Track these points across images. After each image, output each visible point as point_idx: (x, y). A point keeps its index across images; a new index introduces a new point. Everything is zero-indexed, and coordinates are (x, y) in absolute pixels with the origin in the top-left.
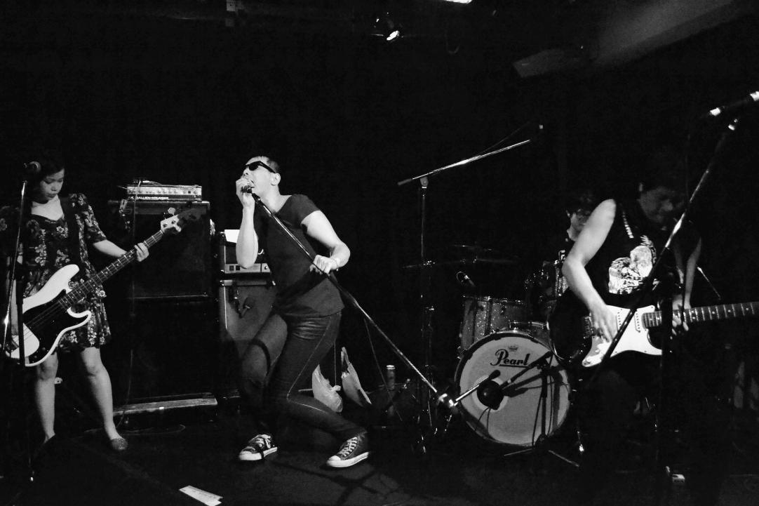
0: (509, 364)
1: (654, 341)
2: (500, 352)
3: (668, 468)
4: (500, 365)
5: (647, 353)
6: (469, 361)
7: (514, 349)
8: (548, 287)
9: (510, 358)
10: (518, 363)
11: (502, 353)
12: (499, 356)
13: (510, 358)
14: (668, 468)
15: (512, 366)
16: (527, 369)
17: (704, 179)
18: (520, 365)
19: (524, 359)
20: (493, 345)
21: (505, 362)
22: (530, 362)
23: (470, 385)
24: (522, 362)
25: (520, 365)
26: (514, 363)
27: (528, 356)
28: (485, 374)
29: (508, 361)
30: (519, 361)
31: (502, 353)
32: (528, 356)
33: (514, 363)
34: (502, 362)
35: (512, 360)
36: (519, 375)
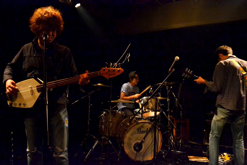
4: (139, 133)
10: (144, 132)
12: (138, 131)
21: (140, 132)
24: (145, 131)
25: (145, 132)
30: (145, 131)
34: (139, 132)
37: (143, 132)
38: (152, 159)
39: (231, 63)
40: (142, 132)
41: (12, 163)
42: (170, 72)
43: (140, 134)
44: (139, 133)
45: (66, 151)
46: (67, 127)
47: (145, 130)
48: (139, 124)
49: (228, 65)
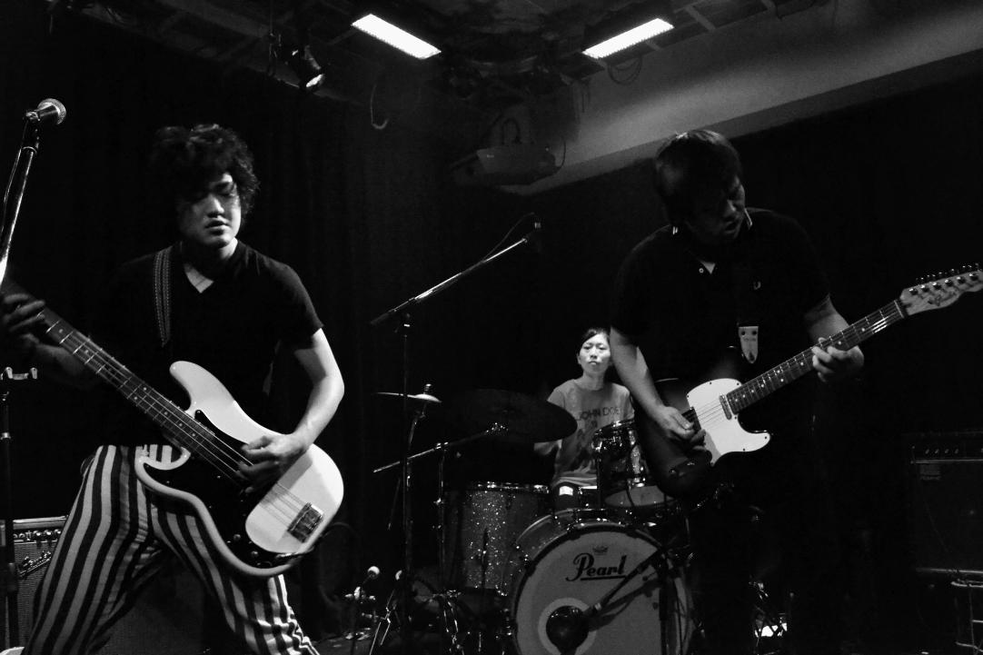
0: (596, 576)
1: (749, 424)
2: (581, 557)
3: (397, 577)
4: (582, 579)
5: (746, 451)
6: (530, 578)
7: (602, 550)
8: (622, 457)
9: (596, 565)
10: (609, 573)
11: (584, 559)
12: (578, 566)
13: (596, 565)
14: (397, 577)
15: (606, 578)
16: (627, 579)
17: (310, 316)
18: (613, 574)
19: (618, 566)
20: (569, 546)
21: (589, 573)
22: (627, 571)
23: (535, 618)
24: (615, 569)
25: (613, 574)
26: (604, 573)
27: (624, 558)
28: (585, 602)
29: (594, 570)
30: (611, 569)
31: (584, 559)
32: (624, 558)
33: (604, 573)
34: (584, 574)
35: (599, 569)
36: (614, 593)
37: (604, 573)
38: (673, 432)
39: (830, 318)
40: (598, 573)
41: (691, 561)
42: (393, 600)
43: (589, 582)
44: (582, 579)
45: (572, 83)
46: (622, 396)
47: (613, 566)
48: (582, 537)
49: (772, 385)
